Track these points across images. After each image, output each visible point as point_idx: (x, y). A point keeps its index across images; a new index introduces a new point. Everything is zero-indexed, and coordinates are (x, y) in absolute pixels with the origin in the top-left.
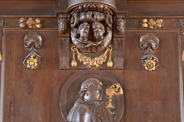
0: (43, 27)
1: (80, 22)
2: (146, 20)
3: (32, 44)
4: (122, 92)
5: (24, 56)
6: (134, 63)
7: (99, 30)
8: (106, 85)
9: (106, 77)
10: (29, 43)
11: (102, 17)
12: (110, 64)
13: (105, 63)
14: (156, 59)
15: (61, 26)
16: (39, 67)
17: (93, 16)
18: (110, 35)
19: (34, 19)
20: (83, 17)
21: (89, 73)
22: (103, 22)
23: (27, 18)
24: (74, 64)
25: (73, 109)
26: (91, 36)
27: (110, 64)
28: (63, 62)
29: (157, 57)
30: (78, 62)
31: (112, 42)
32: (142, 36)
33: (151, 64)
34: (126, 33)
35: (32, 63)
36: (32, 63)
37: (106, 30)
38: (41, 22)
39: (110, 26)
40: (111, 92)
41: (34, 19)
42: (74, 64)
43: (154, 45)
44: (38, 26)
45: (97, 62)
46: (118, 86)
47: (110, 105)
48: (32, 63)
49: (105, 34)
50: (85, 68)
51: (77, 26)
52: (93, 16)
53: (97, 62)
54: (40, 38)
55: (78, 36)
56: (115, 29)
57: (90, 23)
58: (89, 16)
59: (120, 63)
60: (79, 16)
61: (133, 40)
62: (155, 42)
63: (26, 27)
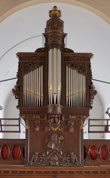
0: (40, 118)
1: (51, 118)
2: (70, 116)
3: (37, 124)
4: (63, 138)
5: (35, 127)
6: (67, 129)
7: (57, 120)
8: (59, 136)
9: (59, 134)
10: (36, 123)
11: (58, 116)
12: (60, 130)
13: (58, 130)
14: (73, 128)
15: (46, 118)
16: (39, 131)
17: (55, 116)
18: (60, 121)
19: (38, 116)
20: (52, 116)
21: (53, 132)
22: (58, 117)
23: (43, 64)
24: (49, 130)
25: (49, 143)
26: (55, 122)
27: (60, 130)
28: (46, 129)
29: (73, 127)
30: (50, 129)
31: (60, 123)
32: (47, 151)
33: (72, 130)
34: (64, 120)
35: (37, 129)
36: (37, 129)
37: (59, 120)
38: (56, 48)
39: (60, 118)
40: (60, 138)
41: (38, 116)
42: (49, 130)
43: (72, 124)
44: (39, 118)
45: (56, 129)
46: (62, 136)
47: (60, 142)
48: (37, 129)
49: (58, 121)
50: (53, 131)
51: (50, 119)
52: (55, 116)
53: (56, 129)
54: (40, 122)
55: (51, 122)
56: (61, 119)
57: (54, 118)
58: (54, 116)
59: (63, 129)
60: (51, 116)
61: (66, 122)
62: (73, 123)
63: (35, 118)
